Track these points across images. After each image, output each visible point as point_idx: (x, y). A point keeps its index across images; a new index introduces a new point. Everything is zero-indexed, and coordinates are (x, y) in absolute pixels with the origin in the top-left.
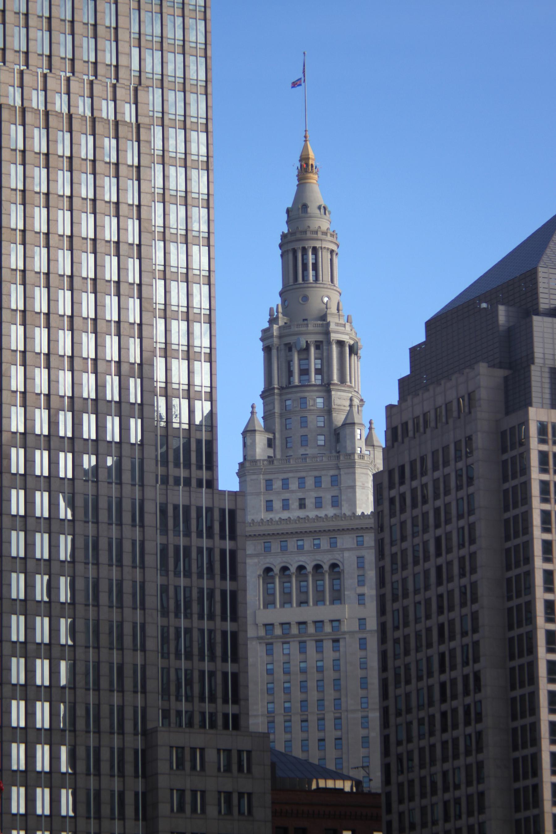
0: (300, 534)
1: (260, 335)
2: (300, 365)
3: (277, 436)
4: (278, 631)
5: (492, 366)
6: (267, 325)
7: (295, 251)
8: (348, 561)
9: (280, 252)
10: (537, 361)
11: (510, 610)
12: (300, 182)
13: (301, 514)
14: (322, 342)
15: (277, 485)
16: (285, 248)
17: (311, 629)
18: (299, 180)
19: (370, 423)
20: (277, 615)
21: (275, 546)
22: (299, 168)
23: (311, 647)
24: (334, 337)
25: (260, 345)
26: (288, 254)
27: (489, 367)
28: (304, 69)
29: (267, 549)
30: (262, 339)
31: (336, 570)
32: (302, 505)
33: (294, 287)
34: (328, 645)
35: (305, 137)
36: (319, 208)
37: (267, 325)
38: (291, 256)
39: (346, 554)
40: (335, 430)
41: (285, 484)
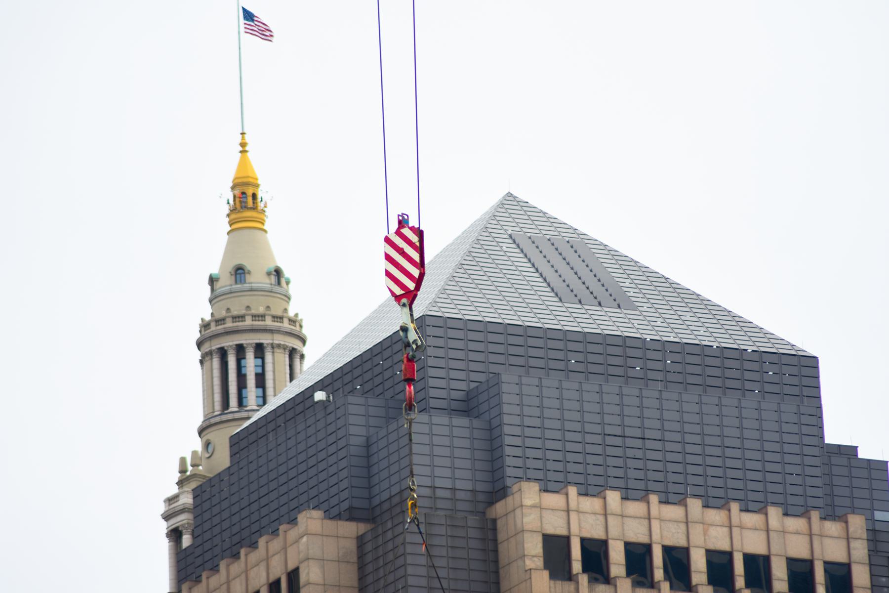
1: (162, 508)
5: (333, 515)
6: (175, 490)
7: (223, 353)
9: (198, 355)
12: (234, 226)
16: (206, 347)
22: (231, 202)
25: (163, 527)
26: (212, 359)
27: (325, 518)
33: (224, 418)
35: (243, 145)
38: (216, 362)
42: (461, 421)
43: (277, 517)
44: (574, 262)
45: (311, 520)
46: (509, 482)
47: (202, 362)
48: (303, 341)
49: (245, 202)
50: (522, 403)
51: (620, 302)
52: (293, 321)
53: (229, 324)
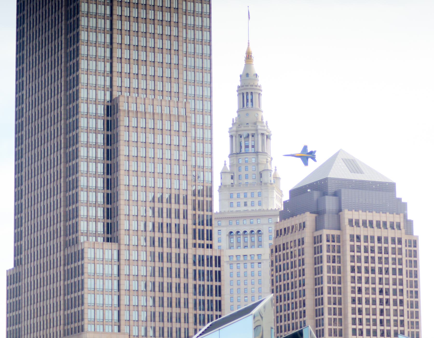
0: (245, 217)
1: (228, 130)
2: (245, 143)
3: (235, 174)
4: (235, 259)
5: (311, 213)
6: (231, 126)
8: (265, 230)
10: (327, 212)
11: (316, 300)
13: (245, 208)
14: (254, 134)
15: (235, 196)
17: (249, 258)
18: (246, 62)
19: (276, 167)
20: (234, 252)
21: (234, 223)
23: (249, 265)
24: (260, 132)
25: (228, 135)
28: (249, 15)
29: (230, 224)
30: (229, 132)
31: (260, 232)
32: (246, 204)
34: (256, 265)
36: (254, 75)
37: (231, 126)
39: (264, 226)
40: (260, 172)
41: (238, 196)
42: (334, 198)
43: (302, 211)
44: (352, 164)
45: (308, 214)
46: (342, 208)
47: (238, 95)
48: (262, 91)
49: (249, 57)
50: (345, 195)
51: (361, 172)
52: (259, 87)
53: (245, 87)
